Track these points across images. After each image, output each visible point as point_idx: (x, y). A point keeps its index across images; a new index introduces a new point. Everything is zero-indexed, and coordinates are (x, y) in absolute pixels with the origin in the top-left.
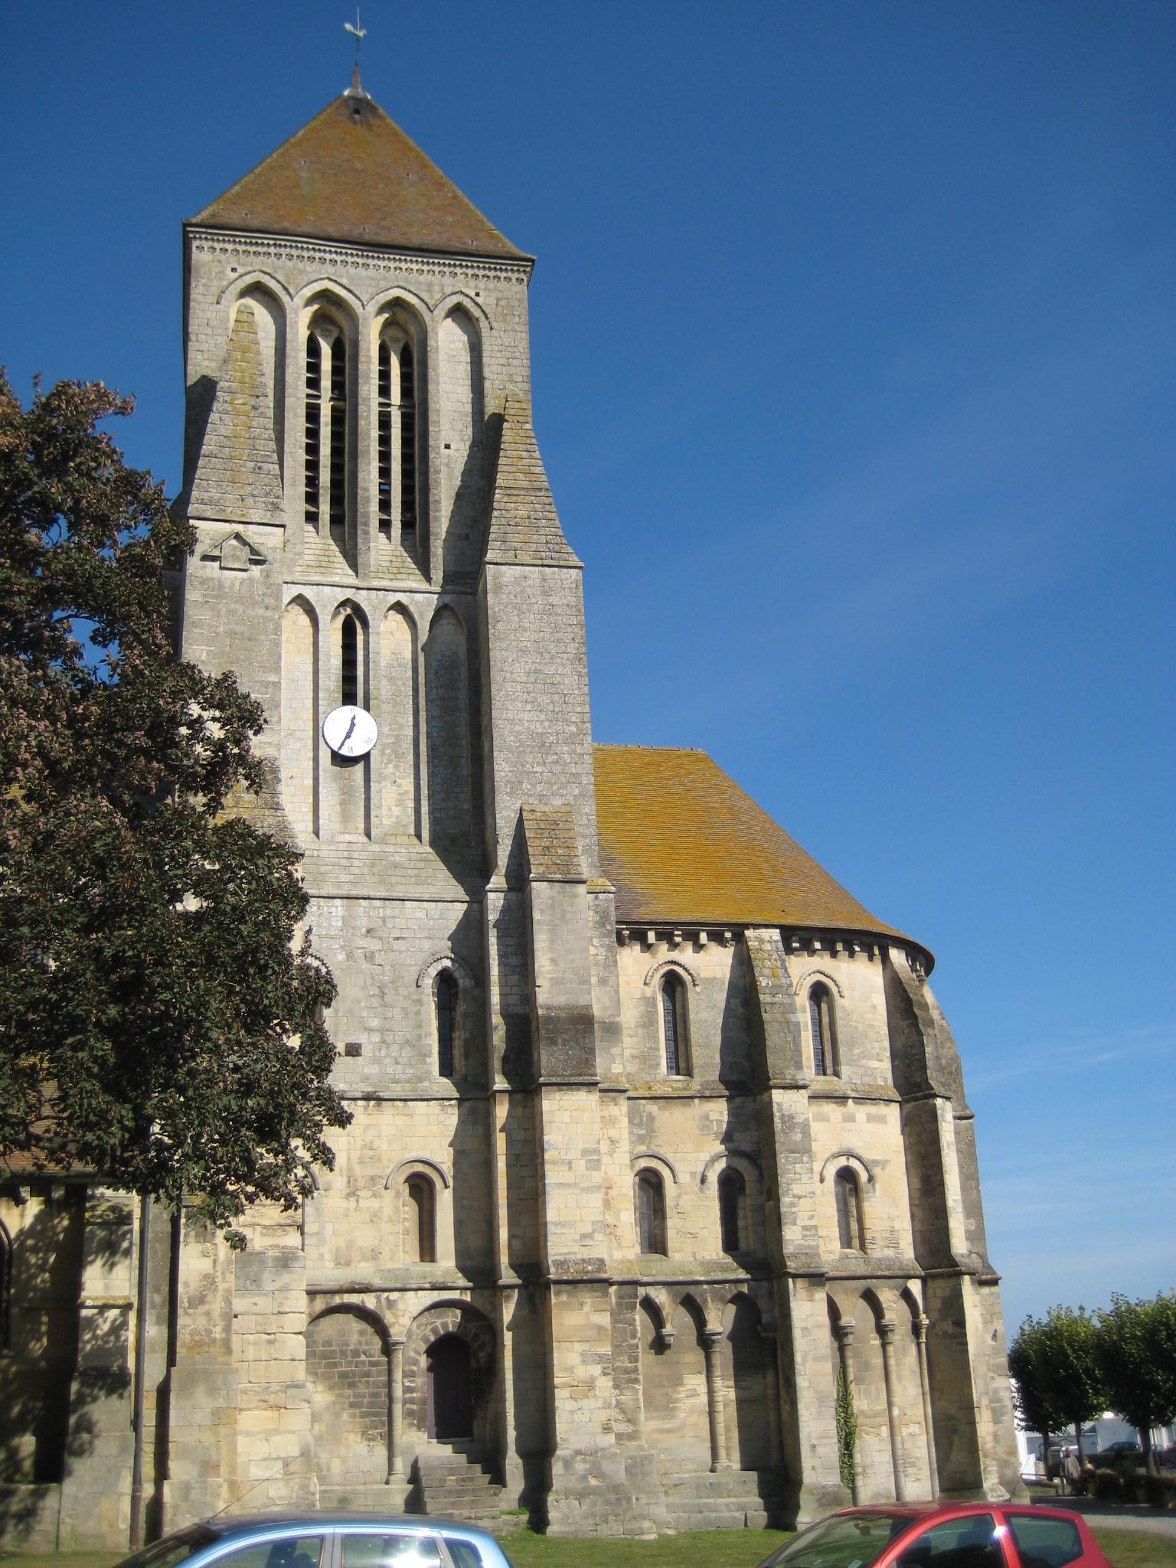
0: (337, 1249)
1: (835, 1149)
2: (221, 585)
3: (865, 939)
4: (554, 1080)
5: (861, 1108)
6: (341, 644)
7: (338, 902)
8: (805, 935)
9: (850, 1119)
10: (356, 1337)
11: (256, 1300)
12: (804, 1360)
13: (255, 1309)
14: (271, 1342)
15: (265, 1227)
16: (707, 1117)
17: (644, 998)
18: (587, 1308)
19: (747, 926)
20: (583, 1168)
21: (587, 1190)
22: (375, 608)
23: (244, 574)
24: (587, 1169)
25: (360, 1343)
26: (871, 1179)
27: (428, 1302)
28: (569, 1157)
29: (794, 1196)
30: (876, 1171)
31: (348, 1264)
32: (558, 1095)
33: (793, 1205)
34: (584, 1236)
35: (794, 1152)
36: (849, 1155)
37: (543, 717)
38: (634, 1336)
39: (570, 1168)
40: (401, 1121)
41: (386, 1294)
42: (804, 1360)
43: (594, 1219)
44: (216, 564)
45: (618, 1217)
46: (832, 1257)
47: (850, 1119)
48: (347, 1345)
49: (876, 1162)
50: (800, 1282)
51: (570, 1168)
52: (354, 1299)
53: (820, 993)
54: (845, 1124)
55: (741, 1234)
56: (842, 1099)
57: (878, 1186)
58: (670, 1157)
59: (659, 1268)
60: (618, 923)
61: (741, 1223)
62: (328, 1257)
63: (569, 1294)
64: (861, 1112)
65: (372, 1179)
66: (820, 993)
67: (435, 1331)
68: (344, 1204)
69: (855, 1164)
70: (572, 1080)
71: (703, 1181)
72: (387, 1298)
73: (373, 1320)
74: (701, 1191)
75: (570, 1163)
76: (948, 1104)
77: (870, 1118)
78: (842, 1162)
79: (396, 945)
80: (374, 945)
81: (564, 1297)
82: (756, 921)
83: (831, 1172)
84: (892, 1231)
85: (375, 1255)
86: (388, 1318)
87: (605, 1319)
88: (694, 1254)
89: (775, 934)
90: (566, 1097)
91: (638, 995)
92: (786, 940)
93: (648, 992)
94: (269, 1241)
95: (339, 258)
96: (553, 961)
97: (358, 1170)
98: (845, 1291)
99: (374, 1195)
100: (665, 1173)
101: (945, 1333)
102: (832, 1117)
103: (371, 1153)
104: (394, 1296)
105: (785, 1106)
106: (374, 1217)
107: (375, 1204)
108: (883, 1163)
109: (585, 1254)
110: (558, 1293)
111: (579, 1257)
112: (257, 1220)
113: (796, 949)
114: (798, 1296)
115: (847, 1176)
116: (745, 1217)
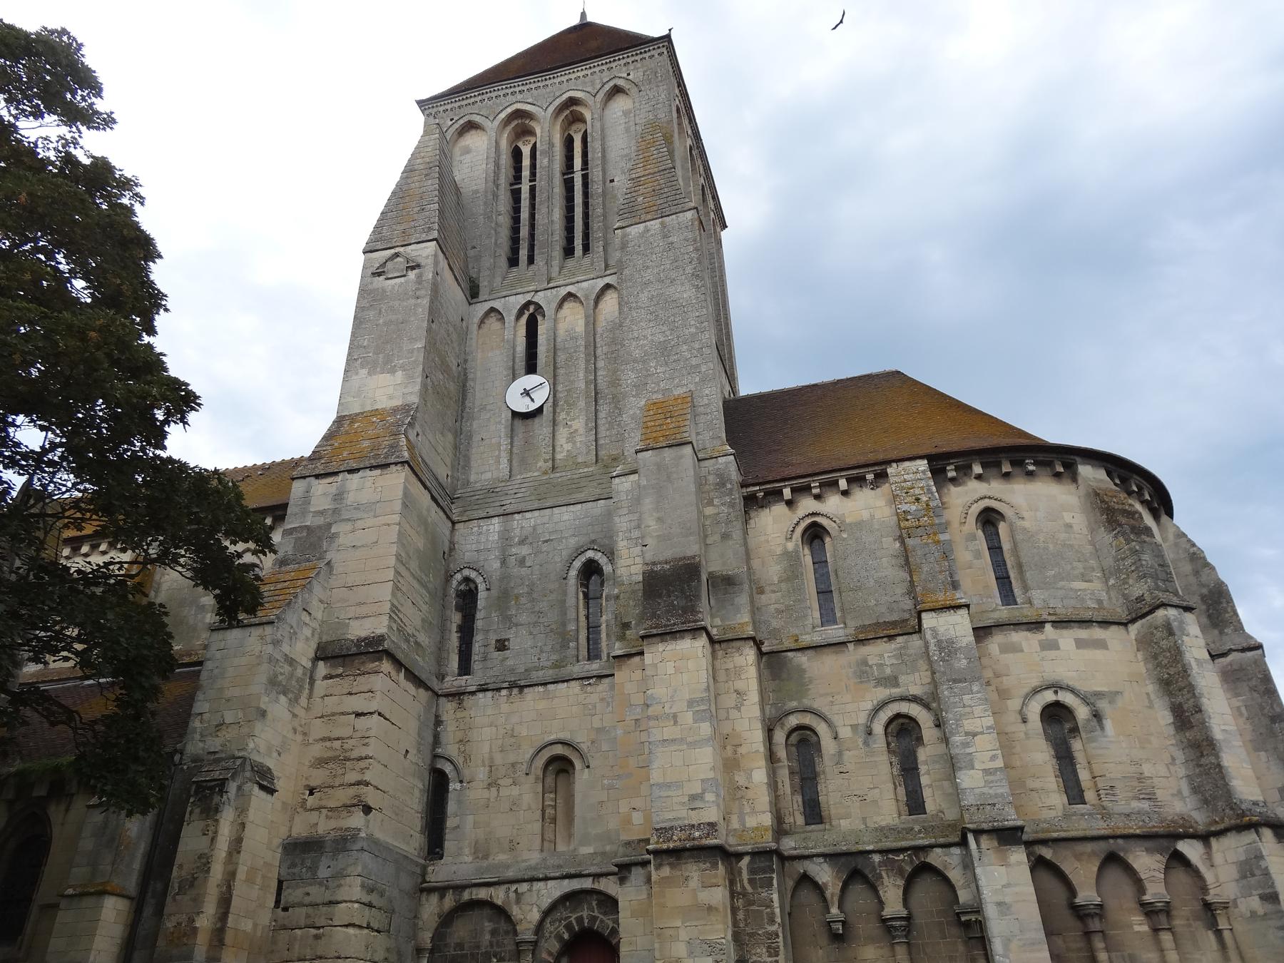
0: (476, 843)
1: (1035, 682)
2: (384, 291)
3: (1041, 457)
4: (654, 631)
5: (1065, 632)
6: (18, 25)
7: (496, 520)
8: (960, 461)
9: (1052, 645)
10: (488, 937)
11: (309, 889)
12: (1007, 942)
13: (307, 900)
14: (317, 937)
15: (331, 810)
16: (864, 662)
17: (785, 553)
18: (694, 883)
19: (889, 462)
20: (690, 721)
21: (693, 745)
22: (549, 303)
23: (402, 280)
24: (695, 721)
25: (491, 945)
26: (1097, 716)
27: (557, 894)
28: (673, 710)
29: (967, 734)
30: (1102, 705)
31: (486, 857)
32: (661, 647)
33: (966, 745)
34: (693, 798)
35: (960, 681)
36: (1056, 687)
37: (665, 328)
38: (772, 921)
39: (676, 723)
40: (542, 705)
41: (514, 887)
42: (1007, 942)
43: (703, 777)
44: (382, 278)
45: (749, 777)
46: (1053, 814)
47: (1052, 645)
48: (478, 947)
49: (1099, 695)
50: (985, 841)
51: (676, 723)
52: (482, 894)
53: (989, 518)
54: (1045, 653)
55: (927, 793)
56: (1037, 625)
57: (1108, 724)
58: (825, 710)
59: (820, 840)
60: (743, 485)
61: (924, 780)
62: (467, 851)
63: (672, 866)
64: (1066, 639)
65: (513, 765)
66: (989, 518)
67: (569, 927)
68: (486, 794)
69: (1067, 698)
70: (676, 628)
71: (870, 733)
72: (516, 891)
73: (501, 913)
74: (866, 743)
75: (675, 716)
76: (1189, 617)
77: (1080, 644)
78: (1049, 696)
79: (545, 547)
80: (525, 550)
81: (666, 871)
82: (894, 455)
83: (1035, 708)
84: (1141, 778)
85: (512, 846)
86: (515, 912)
87: (718, 896)
88: (864, 819)
89: (922, 465)
90: (669, 647)
91: (779, 551)
92: (937, 472)
93: (790, 546)
94: (333, 824)
95: (525, 88)
96: (660, 520)
97: (499, 759)
98: (1078, 857)
99: (514, 783)
100: (822, 728)
101: (1253, 914)
102: (1024, 645)
103: (513, 740)
104: (524, 887)
105: (941, 630)
106: (514, 806)
107: (515, 791)
108: (1113, 696)
109: (695, 818)
110: (658, 867)
111: (686, 822)
112: (323, 803)
113: (953, 480)
114: (985, 859)
115: (1056, 714)
116: (928, 773)
